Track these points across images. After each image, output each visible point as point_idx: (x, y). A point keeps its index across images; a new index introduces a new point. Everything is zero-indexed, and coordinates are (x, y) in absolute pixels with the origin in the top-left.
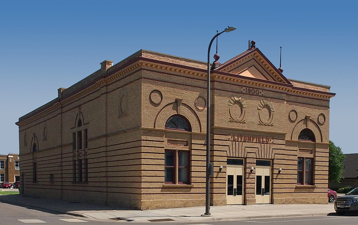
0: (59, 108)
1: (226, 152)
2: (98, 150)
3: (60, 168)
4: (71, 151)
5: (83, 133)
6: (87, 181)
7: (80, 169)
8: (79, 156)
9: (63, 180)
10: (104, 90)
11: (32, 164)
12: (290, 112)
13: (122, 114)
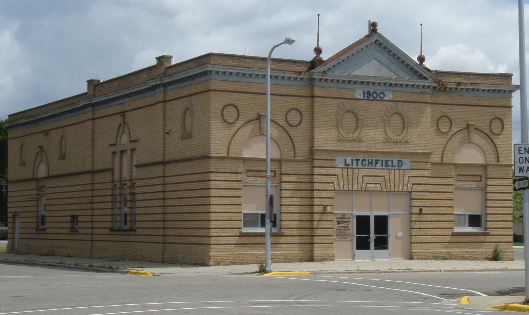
2: (152, 182)
3: (89, 206)
13: (187, 135)
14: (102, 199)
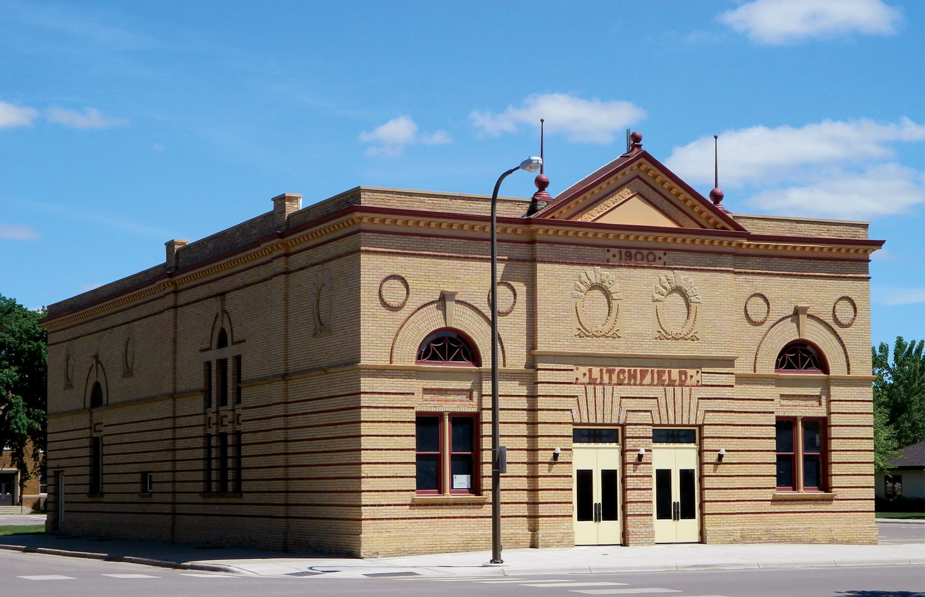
0: (169, 293)
1: (569, 413)
3: (169, 456)
4: (200, 409)
5: (230, 365)
6: (238, 491)
7: (223, 458)
8: (220, 423)
9: (178, 487)
10: (280, 265)
11: (87, 442)
12: (752, 296)
13: (321, 327)
14: (189, 443)
